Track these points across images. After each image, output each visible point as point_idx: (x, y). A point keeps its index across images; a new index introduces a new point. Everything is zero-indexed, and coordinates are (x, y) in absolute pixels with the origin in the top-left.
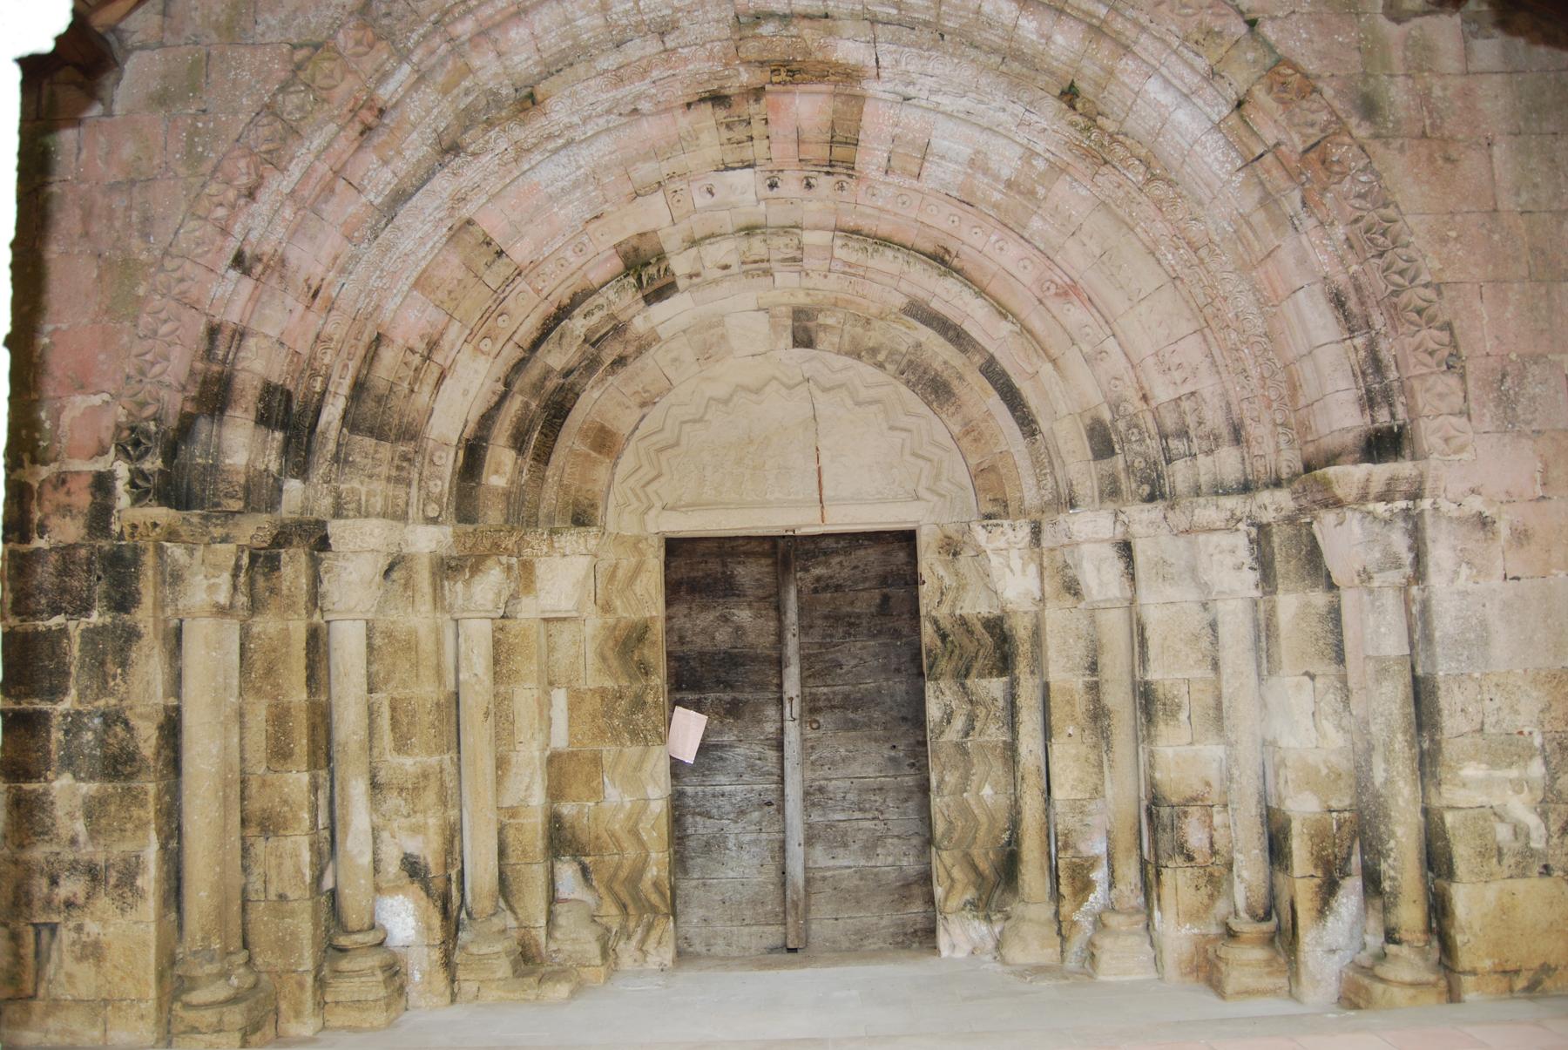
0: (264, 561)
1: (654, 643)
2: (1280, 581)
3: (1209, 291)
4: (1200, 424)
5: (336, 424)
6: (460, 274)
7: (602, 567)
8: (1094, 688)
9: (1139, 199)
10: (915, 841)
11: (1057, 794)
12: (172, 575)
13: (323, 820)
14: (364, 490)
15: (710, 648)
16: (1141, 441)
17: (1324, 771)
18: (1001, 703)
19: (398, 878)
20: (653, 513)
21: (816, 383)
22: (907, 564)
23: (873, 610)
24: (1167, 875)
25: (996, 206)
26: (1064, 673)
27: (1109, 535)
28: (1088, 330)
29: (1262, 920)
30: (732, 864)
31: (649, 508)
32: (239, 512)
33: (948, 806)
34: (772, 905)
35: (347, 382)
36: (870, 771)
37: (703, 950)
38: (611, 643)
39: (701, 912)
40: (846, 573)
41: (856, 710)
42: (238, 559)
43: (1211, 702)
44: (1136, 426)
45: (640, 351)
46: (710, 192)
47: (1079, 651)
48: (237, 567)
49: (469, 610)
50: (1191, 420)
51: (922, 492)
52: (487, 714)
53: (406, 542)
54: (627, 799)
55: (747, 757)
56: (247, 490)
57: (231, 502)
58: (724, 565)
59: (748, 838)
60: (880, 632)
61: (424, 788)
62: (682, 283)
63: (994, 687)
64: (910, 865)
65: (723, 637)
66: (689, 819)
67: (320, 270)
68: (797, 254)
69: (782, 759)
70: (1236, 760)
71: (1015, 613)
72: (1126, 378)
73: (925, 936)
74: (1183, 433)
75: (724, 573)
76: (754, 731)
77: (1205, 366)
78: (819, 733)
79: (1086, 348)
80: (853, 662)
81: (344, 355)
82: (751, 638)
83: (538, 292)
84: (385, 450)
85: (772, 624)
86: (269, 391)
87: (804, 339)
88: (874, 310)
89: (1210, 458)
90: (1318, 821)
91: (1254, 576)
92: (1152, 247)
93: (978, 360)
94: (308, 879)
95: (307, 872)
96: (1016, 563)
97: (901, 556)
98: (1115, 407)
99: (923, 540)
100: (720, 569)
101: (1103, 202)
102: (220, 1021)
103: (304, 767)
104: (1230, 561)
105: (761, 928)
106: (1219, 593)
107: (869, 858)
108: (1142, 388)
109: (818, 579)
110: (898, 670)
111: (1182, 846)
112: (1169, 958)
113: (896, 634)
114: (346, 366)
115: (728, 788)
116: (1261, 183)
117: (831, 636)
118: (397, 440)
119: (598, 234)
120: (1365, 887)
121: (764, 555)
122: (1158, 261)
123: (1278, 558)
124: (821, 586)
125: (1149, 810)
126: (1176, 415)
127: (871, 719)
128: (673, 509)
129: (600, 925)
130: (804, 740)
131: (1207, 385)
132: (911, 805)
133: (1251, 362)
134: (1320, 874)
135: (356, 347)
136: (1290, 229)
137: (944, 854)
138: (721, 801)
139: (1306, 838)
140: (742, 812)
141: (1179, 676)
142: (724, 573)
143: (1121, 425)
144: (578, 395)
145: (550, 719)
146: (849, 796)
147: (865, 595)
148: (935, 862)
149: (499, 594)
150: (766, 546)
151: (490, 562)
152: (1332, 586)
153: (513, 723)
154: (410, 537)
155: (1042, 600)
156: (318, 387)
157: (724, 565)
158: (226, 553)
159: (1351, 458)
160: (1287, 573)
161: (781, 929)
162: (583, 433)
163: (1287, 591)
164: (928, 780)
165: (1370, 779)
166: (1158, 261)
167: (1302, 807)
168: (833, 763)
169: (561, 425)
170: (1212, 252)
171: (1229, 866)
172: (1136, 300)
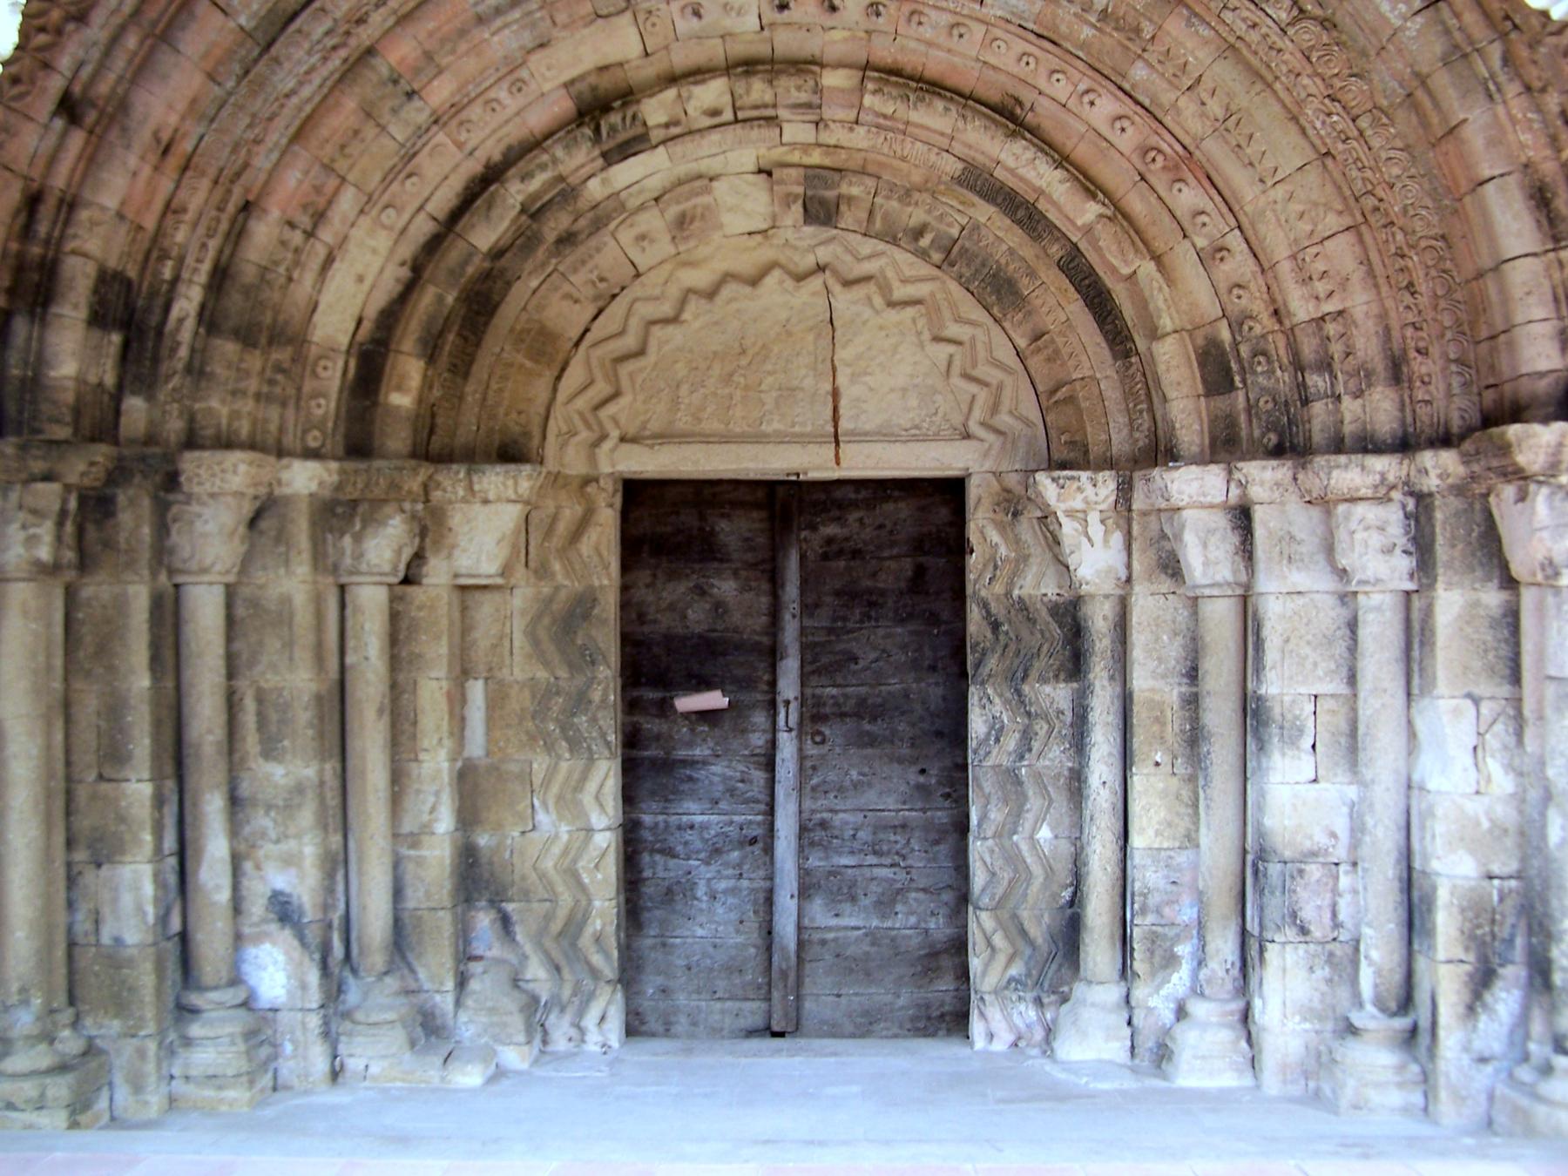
0: (95, 506)
1: (605, 622)
2: (1440, 571)
3: (1369, 174)
4: (1348, 354)
5: (190, 324)
7: (535, 517)
8: (1192, 702)
9: (1280, 44)
10: (947, 896)
11: (1136, 841)
13: (170, 843)
14: (225, 411)
15: (680, 631)
16: (1270, 373)
17: (1486, 824)
18: (1068, 717)
19: (264, 921)
20: (607, 446)
21: (835, 273)
22: (951, 524)
23: (903, 585)
24: (1272, 952)
25: (1084, 45)
26: (1153, 679)
27: (1220, 498)
28: (1204, 218)
29: (1394, 1015)
31: (603, 437)
32: (66, 442)
33: (992, 852)
34: (753, 975)
35: (206, 267)
36: (891, 802)
38: (546, 621)
39: (660, 980)
40: (868, 533)
41: (874, 719)
42: (65, 501)
43: (1344, 726)
44: (1264, 353)
45: (598, 225)
46: (697, 14)
47: (1174, 650)
48: (63, 513)
49: (359, 573)
50: (1336, 349)
51: (974, 427)
53: (279, 482)
54: (564, 828)
55: (725, 778)
56: (77, 411)
58: (702, 517)
59: (722, 885)
60: (911, 616)
61: (299, 806)
62: (656, 135)
63: (1058, 695)
64: (939, 928)
65: (697, 617)
66: (646, 858)
67: (173, 119)
68: (815, 100)
69: (772, 782)
70: (1371, 805)
71: (1092, 596)
72: (1252, 286)
73: (954, 1020)
74: (1325, 365)
75: (701, 529)
76: (735, 744)
77: (1358, 275)
78: (824, 749)
79: (1201, 242)
80: (873, 655)
81: (201, 230)
82: (736, 618)
83: (460, 145)
84: (254, 361)
85: (765, 600)
86: (106, 279)
87: (820, 212)
88: (917, 177)
89: (1360, 401)
90: (1472, 889)
91: (1405, 563)
92: (1295, 110)
93: (1056, 250)
94: (151, 919)
95: (150, 910)
96: (1096, 530)
97: (943, 514)
98: (1238, 324)
99: (973, 491)
100: (696, 524)
101: (1232, 46)
102: (42, 1095)
103: (146, 775)
104: (1376, 540)
105: (738, 1004)
106: (1360, 582)
107: (884, 917)
108: (1273, 301)
109: (830, 541)
110: (933, 668)
111: (1294, 915)
112: (1269, 1061)
113: (933, 619)
114: (204, 246)
115: (699, 819)
116: (1447, 32)
117: (845, 619)
118: (270, 343)
119: (543, 69)
120: (1530, 978)
121: (757, 506)
122: (1303, 131)
123: (1440, 540)
124: (833, 550)
125: (1255, 865)
126: (1315, 341)
127: (894, 732)
129: (525, 991)
130: (802, 757)
131: (1360, 301)
132: (944, 849)
133: (1421, 273)
134: (1471, 957)
135: (218, 220)
136: (1481, 96)
137: (984, 916)
138: (689, 835)
139: (1455, 910)
140: (717, 851)
141: (1303, 690)
142: (701, 529)
143: (1245, 350)
144: (509, 284)
145: (463, 719)
146: (861, 834)
147: (893, 565)
148: (972, 926)
150: (760, 494)
151: (388, 509)
152: (1510, 583)
154: (285, 476)
155: (1129, 580)
156: (167, 273)
157: (702, 517)
158: (48, 494)
159: (1542, 412)
160: (1453, 559)
161: (764, 1005)
163: (1449, 586)
164: (967, 816)
165: (1543, 837)
166: (1303, 131)
167: (1454, 870)
168: (841, 789)
169: (486, 324)
170: (1375, 123)
171: (1356, 943)
172: (1270, 183)
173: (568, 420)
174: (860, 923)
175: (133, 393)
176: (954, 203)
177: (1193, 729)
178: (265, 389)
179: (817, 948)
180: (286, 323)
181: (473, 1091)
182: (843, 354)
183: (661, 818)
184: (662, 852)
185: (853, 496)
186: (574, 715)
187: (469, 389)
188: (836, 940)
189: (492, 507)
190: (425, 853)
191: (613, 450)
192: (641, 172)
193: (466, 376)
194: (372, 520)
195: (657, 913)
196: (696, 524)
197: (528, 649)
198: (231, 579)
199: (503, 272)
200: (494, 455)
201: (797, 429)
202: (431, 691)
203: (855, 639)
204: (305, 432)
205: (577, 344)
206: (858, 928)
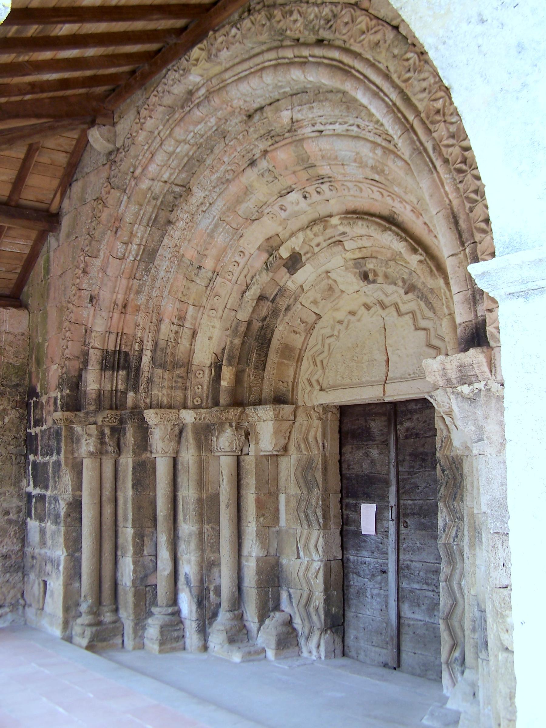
6: (184, 282)
30: (368, 606)
37: (355, 656)
41: (425, 517)
80: (424, 485)
83: (230, 281)
86: (105, 354)
109: (408, 429)
115: (368, 559)
117: (413, 467)
121: (384, 414)
138: (365, 567)
140: (373, 575)
142: (366, 426)
174: (422, 618)
176: (403, 264)
179: (407, 628)
181: (236, 664)
182: (389, 341)
183: (356, 558)
184: (356, 573)
185: (415, 407)
188: (413, 625)
189: (266, 422)
190: (249, 564)
192: (305, 275)
194: (221, 430)
195: (355, 601)
196: (364, 424)
199: (268, 326)
201: (373, 379)
203: (418, 477)
204: (193, 399)
206: (421, 621)
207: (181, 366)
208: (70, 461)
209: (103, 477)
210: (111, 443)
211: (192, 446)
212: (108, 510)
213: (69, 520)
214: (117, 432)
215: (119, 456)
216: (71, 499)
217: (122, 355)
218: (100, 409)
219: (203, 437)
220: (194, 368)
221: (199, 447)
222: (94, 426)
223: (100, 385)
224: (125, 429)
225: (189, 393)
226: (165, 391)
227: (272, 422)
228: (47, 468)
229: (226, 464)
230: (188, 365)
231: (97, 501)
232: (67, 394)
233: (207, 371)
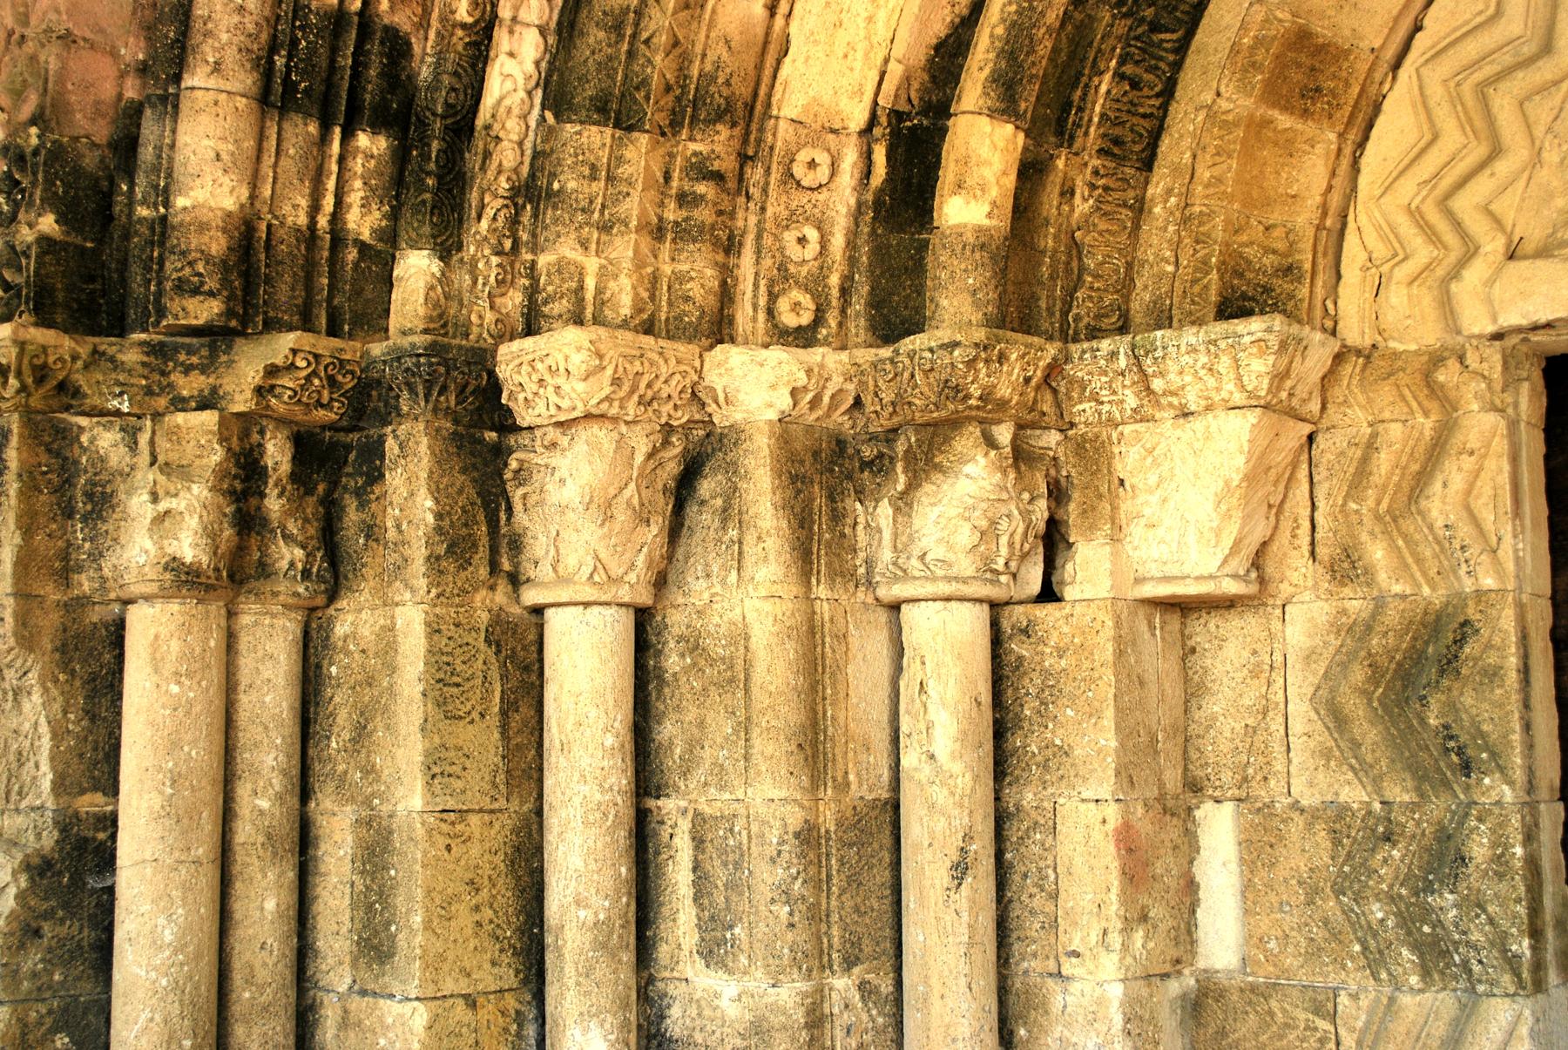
12: (89, 496)
20: (1475, 274)
31: (1471, 251)
38: (1358, 674)
52: (960, 870)
57: (192, 304)
84: (639, 153)
128: (1544, 252)
149: (988, 533)
153: (1054, 896)
162: (1242, 61)
173: (1390, 233)
175: (414, 246)
177: (724, 283)
178: (672, 213)
180: (708, 78)
186: (1429, 889)
187: (1155, 190)
189: (1197, 424)
191: (1490, 282)
193: (1147, 163)
194: (927, 460)
197: (1323, 738)
198: (645, 598)
200: (1211, 311)
202: (1083, 826)
205: (1396, 66)
207: (719, 116)
208: (49, 621)
209: (243, 716)
210: (293, 527)
211: (771, 543)
212: (263, 901)
213: (33, 960)
214: (335, 461)
215: (332, 596)
216: (49, 840)
217: (374, 47)
218: (245, 320)
219: (820, 501)
220: (784, 133)
221: (804, 556)
222: (209, 418)
223: (254, 186)
224: (373, 455)
225: (746, 264)
226: (623, 248)
227: (1252, 417)
228: (463, 191)
229: (946, 640)
230: (746, 111)
231: (204, 850)
232: (45, 241)
233: (850, 158)
